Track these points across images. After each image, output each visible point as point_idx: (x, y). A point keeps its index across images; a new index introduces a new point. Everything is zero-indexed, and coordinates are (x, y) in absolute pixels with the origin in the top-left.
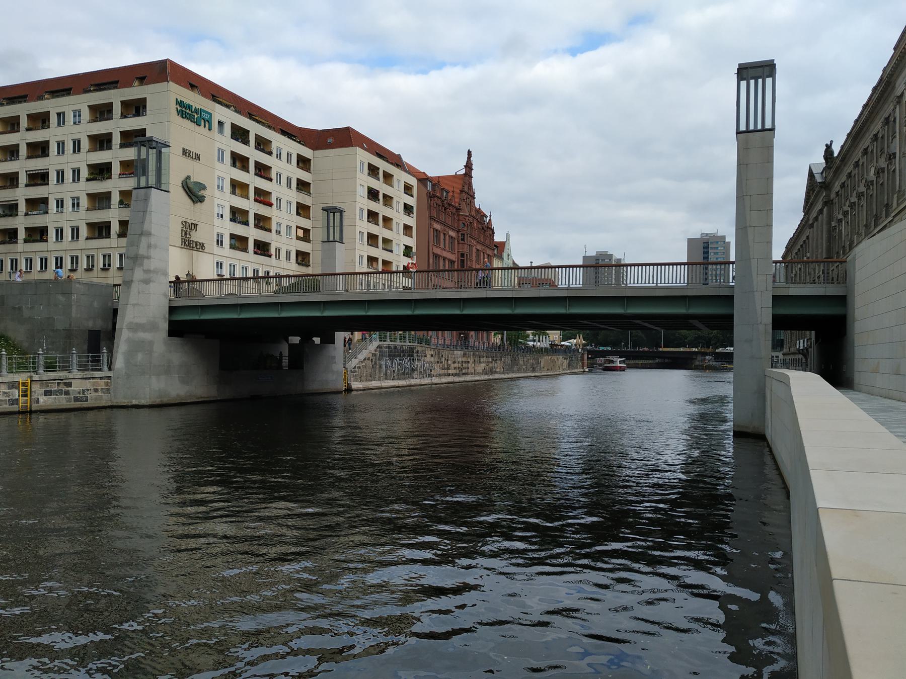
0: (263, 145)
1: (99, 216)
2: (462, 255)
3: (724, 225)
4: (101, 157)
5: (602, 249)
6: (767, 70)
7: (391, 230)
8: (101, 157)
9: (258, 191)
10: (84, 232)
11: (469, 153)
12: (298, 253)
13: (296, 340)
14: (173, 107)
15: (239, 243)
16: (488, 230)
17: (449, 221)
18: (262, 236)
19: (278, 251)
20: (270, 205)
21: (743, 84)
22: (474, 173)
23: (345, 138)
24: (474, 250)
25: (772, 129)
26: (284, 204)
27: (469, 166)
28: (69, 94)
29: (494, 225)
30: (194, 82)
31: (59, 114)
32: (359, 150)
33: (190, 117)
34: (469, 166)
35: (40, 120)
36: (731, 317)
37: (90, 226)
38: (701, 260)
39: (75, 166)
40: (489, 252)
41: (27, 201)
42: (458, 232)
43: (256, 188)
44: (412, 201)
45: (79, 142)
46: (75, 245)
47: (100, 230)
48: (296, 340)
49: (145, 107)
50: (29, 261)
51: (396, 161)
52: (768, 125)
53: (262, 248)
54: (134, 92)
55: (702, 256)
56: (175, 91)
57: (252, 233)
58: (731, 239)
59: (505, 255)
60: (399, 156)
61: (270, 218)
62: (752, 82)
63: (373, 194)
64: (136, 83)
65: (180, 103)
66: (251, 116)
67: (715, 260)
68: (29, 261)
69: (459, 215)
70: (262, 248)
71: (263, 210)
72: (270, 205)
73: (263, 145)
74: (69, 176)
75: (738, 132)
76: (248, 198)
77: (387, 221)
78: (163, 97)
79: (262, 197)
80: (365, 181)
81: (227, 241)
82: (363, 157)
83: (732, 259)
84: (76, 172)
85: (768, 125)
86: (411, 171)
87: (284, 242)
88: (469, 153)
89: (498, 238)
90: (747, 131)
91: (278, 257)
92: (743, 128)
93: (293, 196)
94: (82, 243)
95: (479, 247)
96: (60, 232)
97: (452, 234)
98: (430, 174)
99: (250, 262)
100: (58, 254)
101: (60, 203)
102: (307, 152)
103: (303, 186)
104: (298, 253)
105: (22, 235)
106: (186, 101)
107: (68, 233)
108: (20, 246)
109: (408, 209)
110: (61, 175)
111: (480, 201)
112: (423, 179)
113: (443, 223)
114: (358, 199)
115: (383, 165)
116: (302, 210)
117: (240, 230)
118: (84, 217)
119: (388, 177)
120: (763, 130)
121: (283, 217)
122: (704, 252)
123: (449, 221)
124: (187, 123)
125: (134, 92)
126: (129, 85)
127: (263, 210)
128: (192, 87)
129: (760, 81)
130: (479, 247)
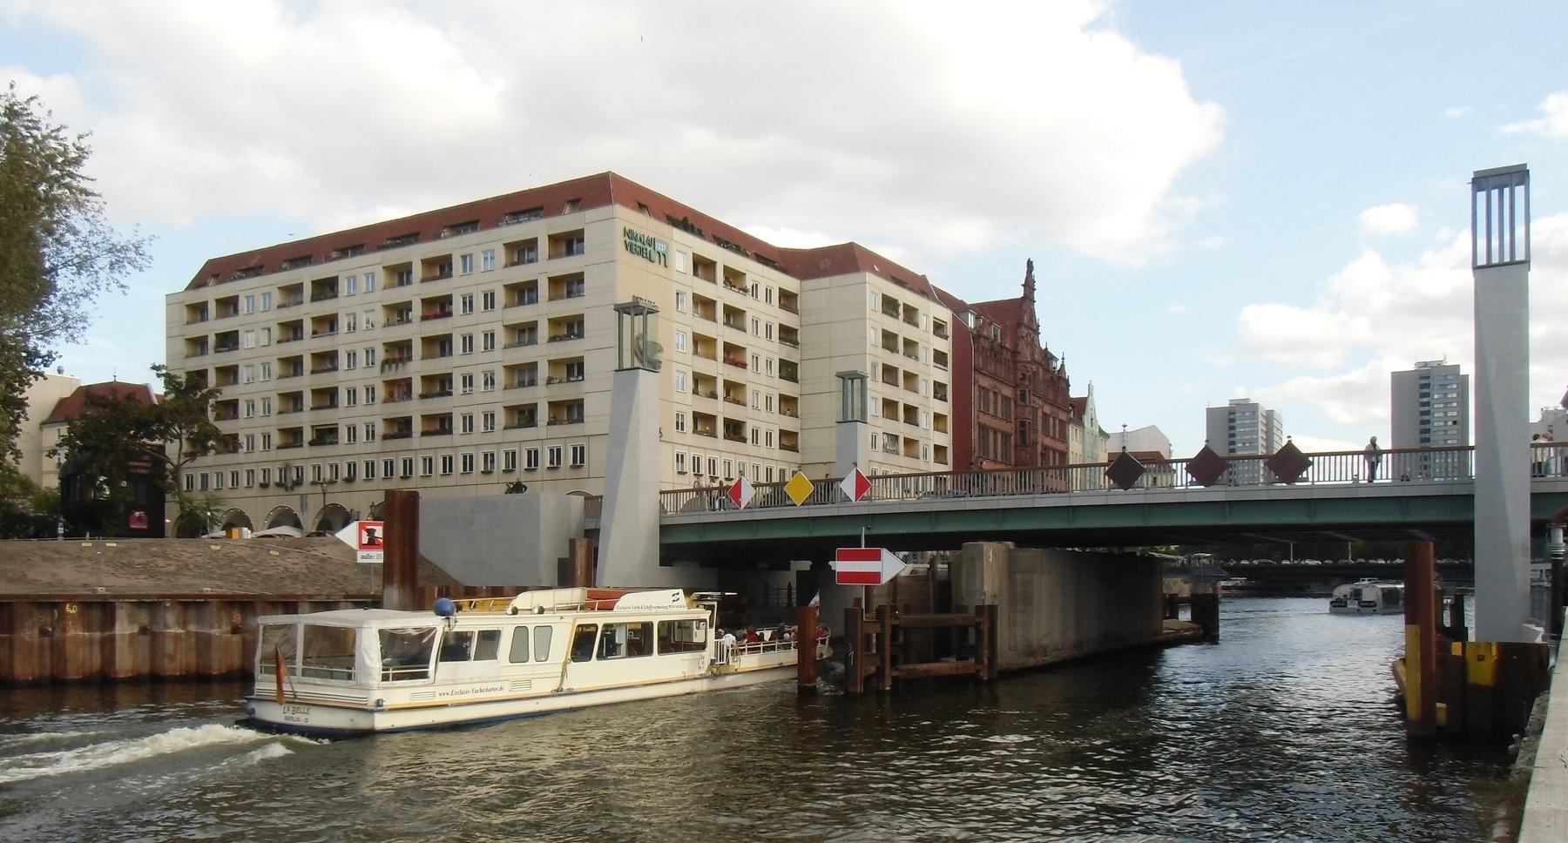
0: (733, 278)
1: (522, 397)
2: (1023, 424)
3: (1455, 347)
4: (523, 314)
5: (1240, 394)
6: (1515, 178)
7: (916, 392)
8: (523, 314)
9: (729, 348)
10: (501, 419)
11: (1030, 265)
12: (783, 433)
13: (806, 565)
14: (620, 239)
15: (703, 422)
16: (1059, 381)
17: (1001, 372)
18: (734, 412)
19: (755, 433)
20: (743, 366)
21: (1482, 195)
22: (1037, 295)
23: (844, 260)
24: (1040, 414)
25: (1526, 262)
26: (762, 363)
27: (1029, 285)
28: (474, 229)
29: (1069, 372)
30: (645, 201)
31: (464, 258)
32: (870, 277)
33: (641, 252)
34: (1029, 285)
35: (441, 267)
36: (1469, 526)
37: (510, 410)
38: (1416, 445)
39: (488, 327)
40: (1063, 416)
41: (218, 301)
42: (1015, 387)
43: (725, 344)
44: (945, 346)
45: (492, 295)
46: (488, 438)
47: (524, 416)
48: (806, 565)
49: (581, 240)
50: (429, 462)
51: (920, 285)
52: (1520, 256)
53: (734, 430)
54: (565, 222)
55: (1418, 437)
56: (625, 217)
57: (722, 409)
58: (1468, 369)
59: (1086, 419)
60: (923, 279)
61: (742, 386)
62: (1495, 193)
63: (889, 339)
64: (567, 209)
65: (629, 233)
66: (718, 241)
67: (1441, 444)
68: (429, 462)
69: (1015, 362)
70: (734, 430)
71: (735, 374)
72: (743, 366)
73: (733, 278)
74: (479, 342)
75: (1476, 268)
76: (715, 359)
77: (910, 377)
78: (607, 226)
79: (733, 354)
80: (878, 321)
81: (689, 422)
82: (876, 286)
83: (1472, 442)
84: (490, 337)
85: (1520, 256)
86: (944, 299)
87: (763, 419)
88: (1030, 265)
89: (1075, 392)
90: (1489, 266)
91: (755, 440)
92: (1482, 261)
93: (776, 350)
94: (499, 434)
95: (1047, 409)
96: (469, 422)
97: (1007, 392)
98: (970, 300)
99: (719, 448)
100: (467, 451)
101: (468, 381)
102: (791, 284)
103: (788, 334)
104: (783, 433)
105: (417, 426)
106: (637, 230)
107: (479, 422)
108: (416, 441)
109: (940, 357)
110: (468, 341)
111: (1047, 339)
112: (958, 307)
113: (993, 377)
114: (869, 349)
115: (904, 296)
116: (788, 370)
117: (706, 406)
118: (502, 398)
119: (911, 315)
120: (1513, 263)
121: (762, 383)
122: (1421, 391)
123: (1001, 372)
124: (639, 260)
125: (565, 222)
126: (557, 211)
127: (735, 374)
128: (641, 207)
129: (1507, 191)
130: (1047, 409)
